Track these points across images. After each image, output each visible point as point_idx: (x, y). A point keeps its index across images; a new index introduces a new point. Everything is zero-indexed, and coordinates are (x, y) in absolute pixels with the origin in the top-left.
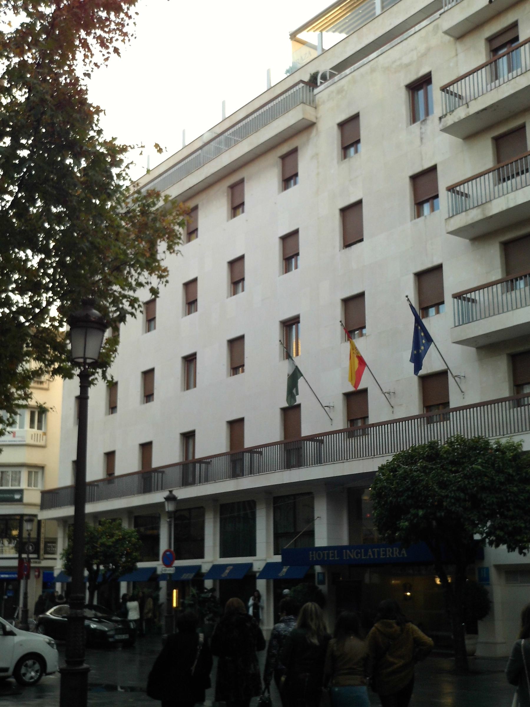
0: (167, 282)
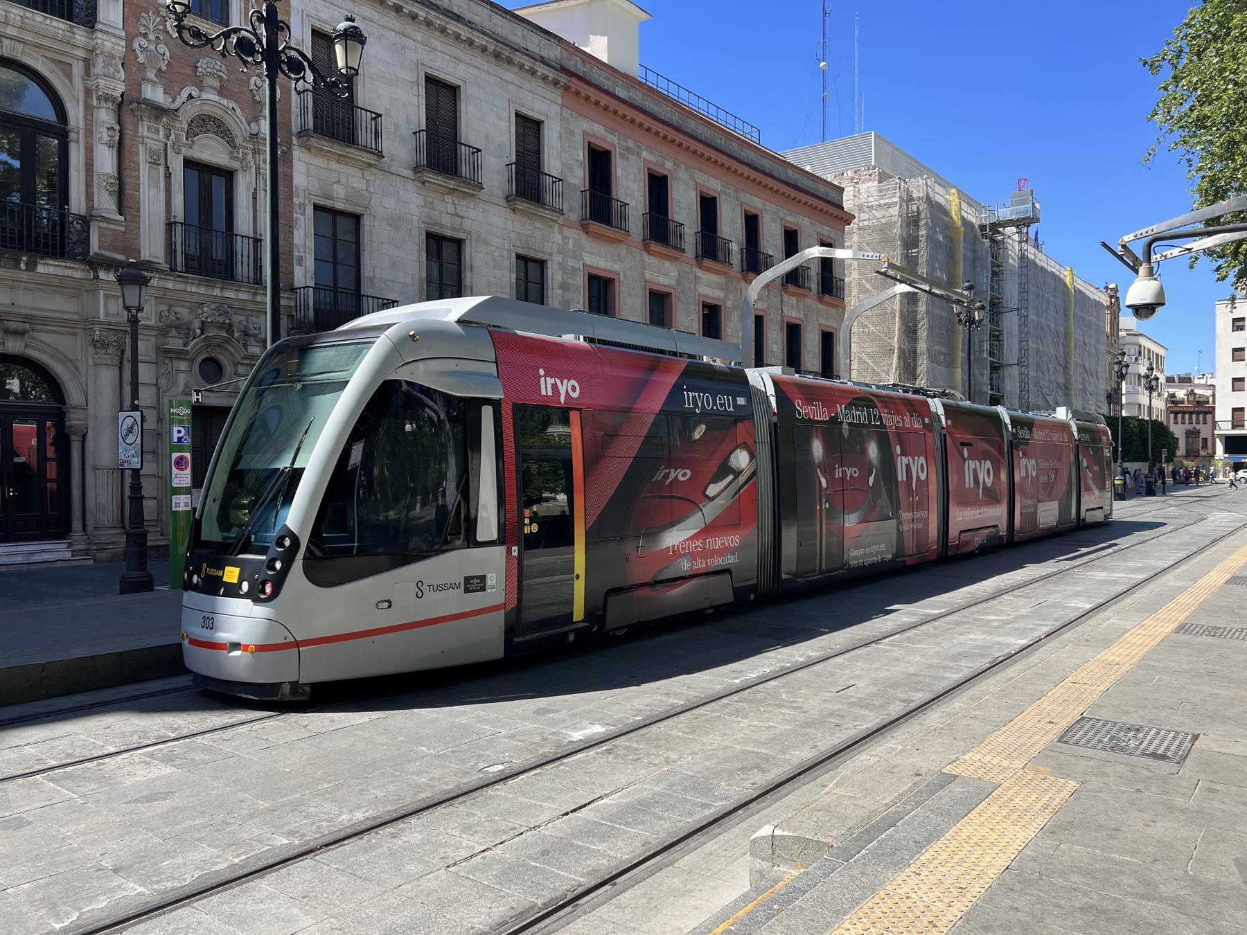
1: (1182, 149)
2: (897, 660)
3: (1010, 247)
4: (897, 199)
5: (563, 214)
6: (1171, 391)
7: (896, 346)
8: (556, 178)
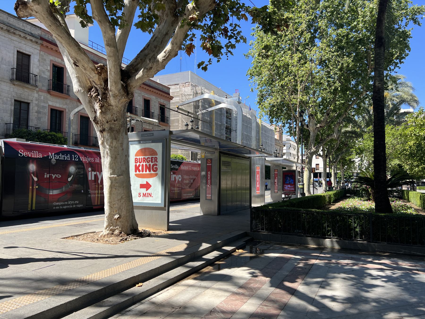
0: (249, 7)
4: (192, 93)
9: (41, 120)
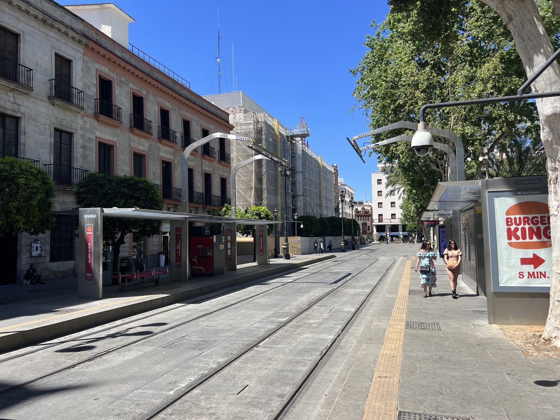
1: (364, 108)
2: (270, 359)
3: (298, 146)
4: (252, 121)
5: (84, 110)
6: (356, 207)
7: (253, 186)
8: (79, 90)
9: (88, 160)
